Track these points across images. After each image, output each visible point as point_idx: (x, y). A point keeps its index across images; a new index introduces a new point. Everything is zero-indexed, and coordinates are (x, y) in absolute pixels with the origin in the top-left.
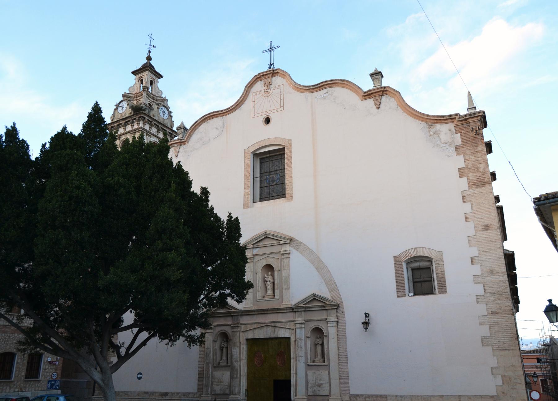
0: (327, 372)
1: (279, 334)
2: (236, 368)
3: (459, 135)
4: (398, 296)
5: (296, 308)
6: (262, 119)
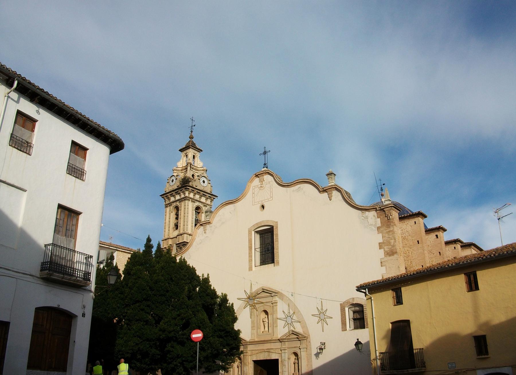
3: (379, 219)
4: (343, 331)
6: (259, 205)
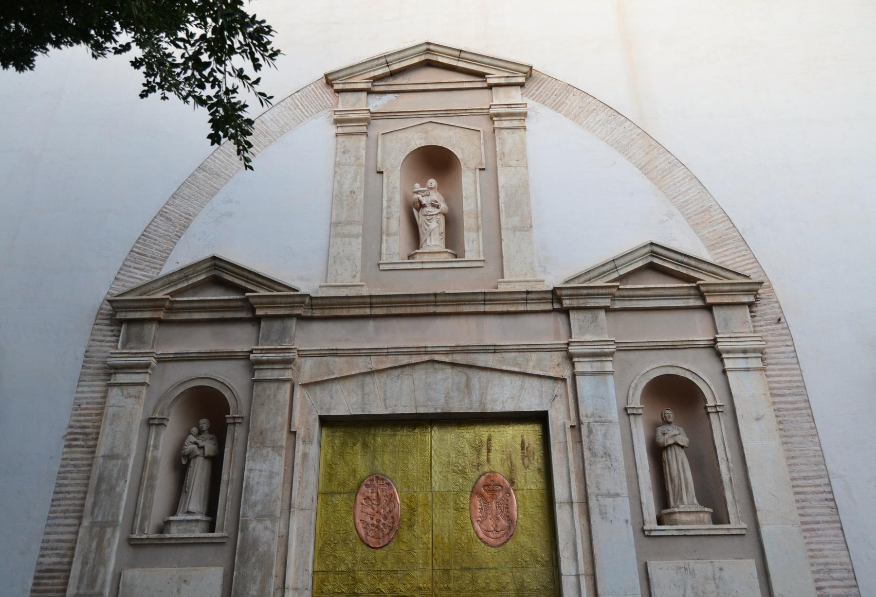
0: (750, 566)
1: (489, 397)
2: (262, 549)
5: (577, 293)
